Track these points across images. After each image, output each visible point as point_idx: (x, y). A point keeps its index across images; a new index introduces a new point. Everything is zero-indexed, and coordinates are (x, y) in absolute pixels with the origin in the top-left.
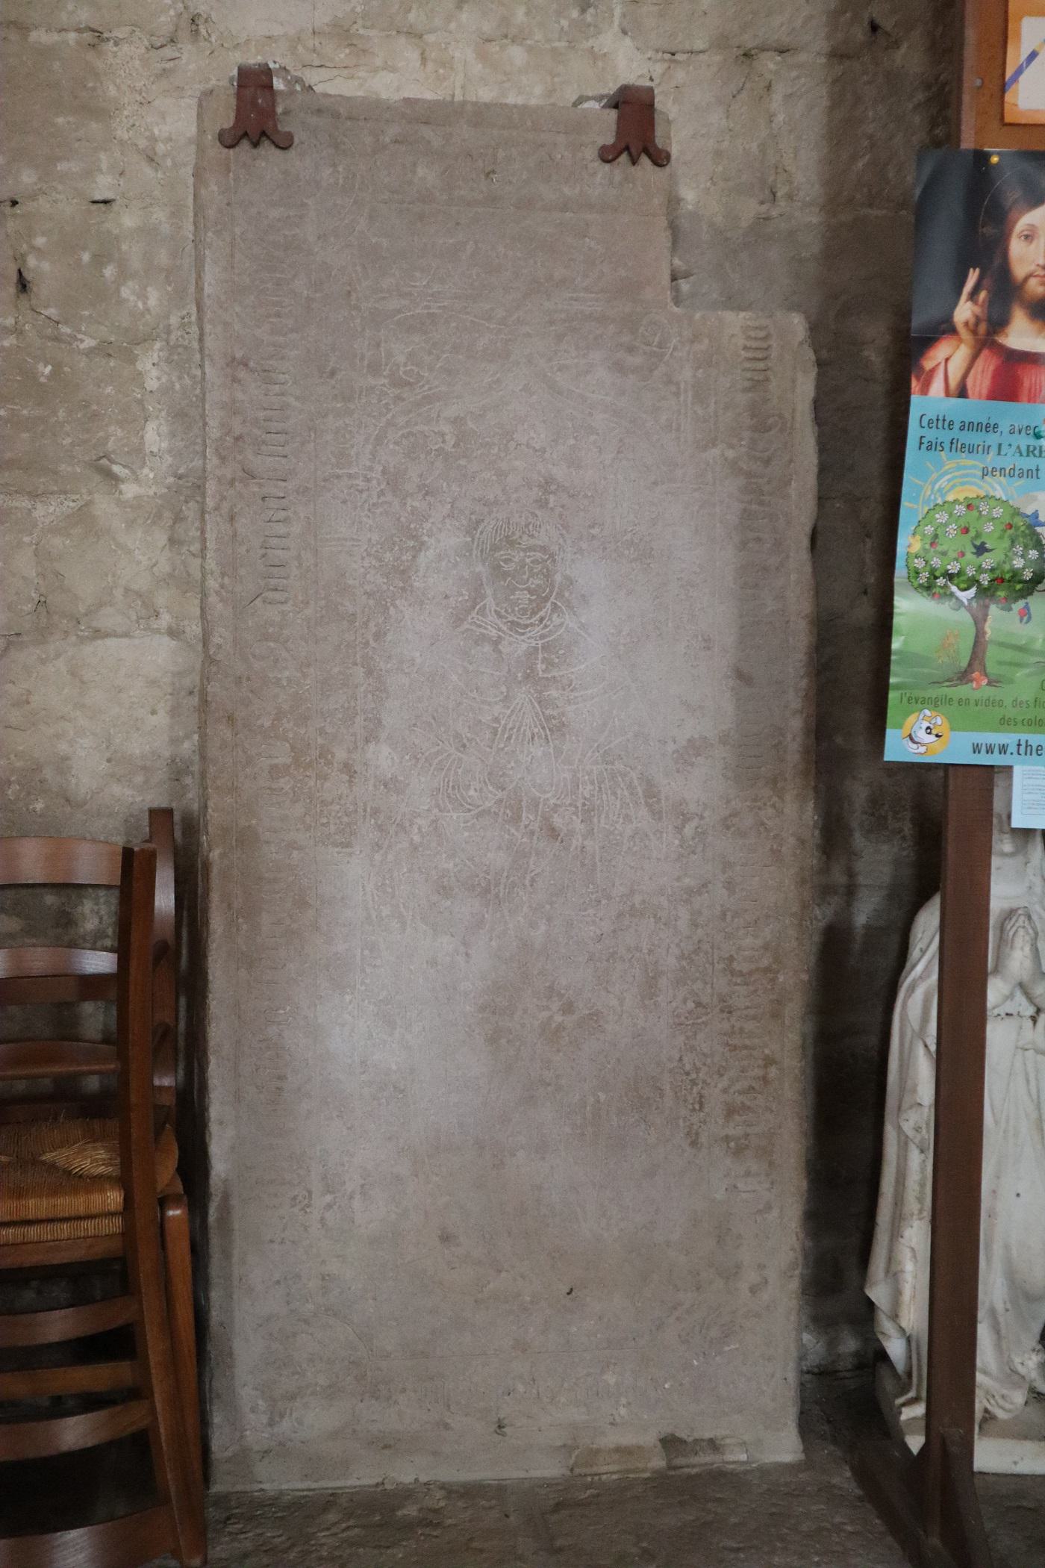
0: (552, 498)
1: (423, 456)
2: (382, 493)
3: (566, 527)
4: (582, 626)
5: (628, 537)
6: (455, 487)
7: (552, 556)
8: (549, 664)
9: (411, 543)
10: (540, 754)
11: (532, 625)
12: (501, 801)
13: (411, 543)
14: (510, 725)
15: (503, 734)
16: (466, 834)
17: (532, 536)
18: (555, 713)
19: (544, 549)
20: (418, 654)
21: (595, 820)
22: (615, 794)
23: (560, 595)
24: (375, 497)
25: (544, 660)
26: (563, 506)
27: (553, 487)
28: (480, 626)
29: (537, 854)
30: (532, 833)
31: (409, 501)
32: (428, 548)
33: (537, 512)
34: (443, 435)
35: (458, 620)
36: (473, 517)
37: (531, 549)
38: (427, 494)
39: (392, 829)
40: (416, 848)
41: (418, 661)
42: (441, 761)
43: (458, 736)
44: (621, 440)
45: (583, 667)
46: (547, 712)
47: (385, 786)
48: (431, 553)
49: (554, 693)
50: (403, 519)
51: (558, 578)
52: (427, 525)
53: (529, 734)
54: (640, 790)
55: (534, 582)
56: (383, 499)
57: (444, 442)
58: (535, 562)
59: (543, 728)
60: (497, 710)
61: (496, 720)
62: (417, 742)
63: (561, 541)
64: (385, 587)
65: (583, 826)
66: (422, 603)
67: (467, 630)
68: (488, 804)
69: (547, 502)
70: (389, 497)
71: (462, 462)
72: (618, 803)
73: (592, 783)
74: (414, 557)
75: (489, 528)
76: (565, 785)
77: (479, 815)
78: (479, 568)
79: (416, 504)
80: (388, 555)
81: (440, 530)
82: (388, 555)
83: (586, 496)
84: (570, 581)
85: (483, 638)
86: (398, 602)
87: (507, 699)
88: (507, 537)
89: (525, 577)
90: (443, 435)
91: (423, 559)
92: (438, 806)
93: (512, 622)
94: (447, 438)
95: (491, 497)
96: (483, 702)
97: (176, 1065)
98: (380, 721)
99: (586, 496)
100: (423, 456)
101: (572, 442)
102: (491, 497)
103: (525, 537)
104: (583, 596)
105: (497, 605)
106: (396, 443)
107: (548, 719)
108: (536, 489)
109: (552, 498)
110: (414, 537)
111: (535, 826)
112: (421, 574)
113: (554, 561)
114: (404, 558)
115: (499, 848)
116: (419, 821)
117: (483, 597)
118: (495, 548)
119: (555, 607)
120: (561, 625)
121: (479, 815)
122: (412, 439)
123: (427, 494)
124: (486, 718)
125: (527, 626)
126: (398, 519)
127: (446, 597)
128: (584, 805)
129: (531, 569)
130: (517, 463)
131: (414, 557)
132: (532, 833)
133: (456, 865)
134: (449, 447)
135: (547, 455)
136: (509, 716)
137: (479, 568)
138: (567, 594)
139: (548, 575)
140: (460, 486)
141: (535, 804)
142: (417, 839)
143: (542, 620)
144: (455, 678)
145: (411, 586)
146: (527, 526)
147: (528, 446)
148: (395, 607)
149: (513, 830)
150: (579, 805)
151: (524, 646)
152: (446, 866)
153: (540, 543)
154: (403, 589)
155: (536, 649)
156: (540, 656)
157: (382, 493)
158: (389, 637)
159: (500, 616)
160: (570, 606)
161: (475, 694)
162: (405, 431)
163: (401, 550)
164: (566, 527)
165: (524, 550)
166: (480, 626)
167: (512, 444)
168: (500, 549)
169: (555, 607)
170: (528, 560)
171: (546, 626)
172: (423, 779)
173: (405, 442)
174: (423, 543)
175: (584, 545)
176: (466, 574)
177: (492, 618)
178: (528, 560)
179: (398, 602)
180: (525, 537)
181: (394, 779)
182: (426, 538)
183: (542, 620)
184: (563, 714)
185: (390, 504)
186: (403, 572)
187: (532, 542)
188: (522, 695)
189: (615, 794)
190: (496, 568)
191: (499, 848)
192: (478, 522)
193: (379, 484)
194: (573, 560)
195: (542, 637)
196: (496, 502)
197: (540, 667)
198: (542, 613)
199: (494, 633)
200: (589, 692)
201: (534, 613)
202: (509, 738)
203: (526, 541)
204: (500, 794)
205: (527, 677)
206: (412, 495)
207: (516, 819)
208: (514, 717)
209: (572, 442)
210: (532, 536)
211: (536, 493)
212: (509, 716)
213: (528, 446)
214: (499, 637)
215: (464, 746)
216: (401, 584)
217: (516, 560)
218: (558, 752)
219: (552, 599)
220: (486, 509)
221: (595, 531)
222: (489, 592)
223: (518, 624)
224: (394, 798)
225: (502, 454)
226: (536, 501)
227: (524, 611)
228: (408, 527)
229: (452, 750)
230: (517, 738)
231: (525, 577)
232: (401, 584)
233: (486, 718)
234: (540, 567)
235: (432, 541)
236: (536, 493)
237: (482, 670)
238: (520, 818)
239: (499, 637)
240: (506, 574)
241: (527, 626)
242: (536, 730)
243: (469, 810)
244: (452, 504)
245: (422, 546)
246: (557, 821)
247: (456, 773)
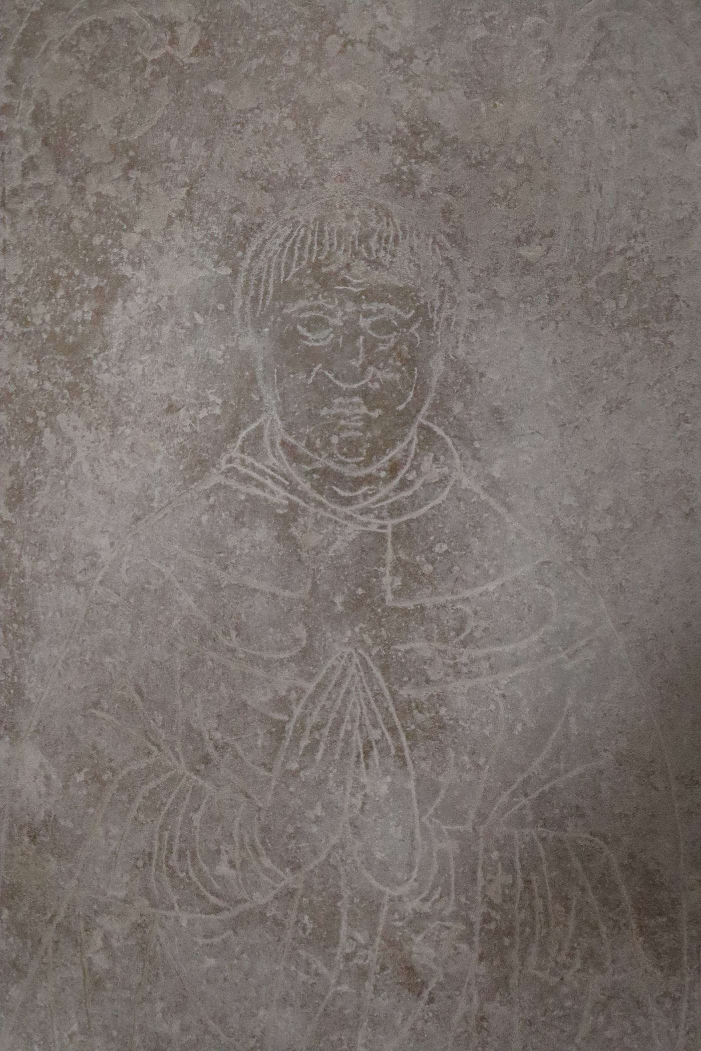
0: (426, 173)
1: (125, 78)
2: (30, 166)
3: (458, 239)
4: (493, 486)
5: (615, 266)
6: (196, 149)
7: (421, 311)
8: (411, 575)
9: (94, 282)
10: (384, 789)
11: (370, 479)
12: (291, 893)
13: (94, 282)
14: (310, 722)
15: (296, 740)
16: (211, 962)
17: (376, 264)
18: (422, 694)
19: (403, 296)
20: (104, 541)
21: (514, 957)
22: (565, 899)
23: (440, 408)
24: (17, 174)
25: (399, 566)
26: (452, 190)
27: (430, 145)
28: (247, 479)
29: (374, 1023)
30: (363, 974)
31: (92, 181)
32: (129, 295)
33: (394, 207)
34: (172, 25)
35: (200, 465)
36: (238, 218)
37: (370, 294)
38: (130, 166)
39: (49, 935)
40: (98, 984)
41: (106, 556)
42: (152, 792)
43: (192, 735)
44: (601, 25)
45: (491, 587)
46: (405, 692)
47: (33, 838)
48: (137, 304)
49: (422, 647)
50: (76, 225)
51: (438, 366)
52: (132, 238)
53: (357, 740)
54: (625, 894)
55: (381, 376)
56: (33, 179)
57: (174, 41)
58: (382, 326)
59: (393, 730)
60: (284, 680)
61: (282, 704)
62: (102, 743)
63: (446, 274)
64: (34, 384)
65: (482, 969)
66: (115, 424)
67: (218, 487)
68: (259, 899)
69: (414, 179)
70: (47, 175)
71: (216, 88)
72: (572, 923)
73: (509, 868)
74: (99, 313)
75: (274, 245)
76: (443, 870)
77: (239, 923)
78: (249, 341)
79: (108, 189)
80: (41, 308)
81: (160, 250)
82: (41, 308)
83: (510, 165)
84: (464, 375)
85: (256, 508)
86: (61, 418)
87: (307, 656)
88: (317, 266)
89: (356, 363)
90: (172, 25)
91: (121, 318)
92: (147, 893)
93: (326, 473)
94: (183, 31)
95: (282, 171)
96: (252, 660)
97: (428, 519)
98: (20, 691)
99: (510, 165)
100: (125, 78)
101: (479, 32)
102: (282, 171)
103: (359, 267)
104: (496, 411)
105: (289, 429)
106: (65, 49)
107: (406, 708)
108: (386, 150)
109: (426, 173)
110: (102, 268)
111: (372, 958)
112: (114, 351)
113: (428, 325)
114: (77, 315)
115: (285, 1001)
116: (103, 920)
117: (256, 410)
118: (286, 292)
119: (428, 438)
120: (443, 481)
121: (239, 923)
122: (102, 38)
123: (130, 166)
124: (260, 698)
125: (358, 482)
126: (67, 226)
127: (172, 409)
128: (487, 919)
129: (371, 345)
130: (346, 87)
131: (99, 313)
132: (363, 974)
133: (185, 1030)
134: (184, 56)
135: (418, 66)
136: (313, 698)
137: (249, 341)
138: (457, 407)
139: (411, 361)
140: (209, 145)
141: (370, 907)
142: (101, 962)
143: (393, 469)
144: (187, 600)
145: (92, 381)
146: (364, 238)
147: (372, 45)
148: (56, 429)
149: (318, 964)
150: (476, 917)
151: (352, 530)
152: (164, 1028)
153: (395, 281)
154: (74, 390)
155: (380, 538)
156: (390, 556)
157: (30, 166)
158: (42, 498)
159: (294, 456)
160: (463, 437)
161: (233, 641)
162: (87, 20)
163: (68, 296)
164: (458, 239)
165: (357, 299)
166: (247, 479)
167: (333, 44)
168: (299, 294)
169: (428, 438)
170: (364, 323)
171: (404, 484)
172: (115, 831)
173: (85, 45)
174: (121, 280)
175: (504, 287)
176: (217, 354)
177: (276, 460)
178: (364, 323)
179: (61, 418)
180: (359, 267)
181: (50, 822)
182: (127, 270)
183: (393, 469)
184: (442, 699)
185: (49, 189)
186: (74, 349)
187: (378, 277)
188: (342, 647)
189: (565, 899)
190: (287, 340)
191: (285, 1001)
192: (248, 232)
193: (25, 145)
194: (474, 325)
195: (396, 509)
196: (292, 182)
197: (389, 582)
198: (395, 453)
199: (280, 496)
200: (508, 648)
201: (376, 452)
202: (312, 748)
203: (360, 276)
204: (288, 879)
205: (356, 604)
206: (99, 167)
207: (324, 937)
208: (323, 700)
209: (479, 32)
210: (376, 264)
211: (388, 158)
212: (313, 698)
213: (372, 45)
214: (292, 506)
215: (206, 760)
216: (69, 378)
217: (337, 321)
218: (428, 789)
219: (420, 419)
220: (269, 199)
221: (531, 252)
222: (270, 397)
223: (339, 478)
224: (53, 865)
225: (310, 67)
226: (387, 179)
227: (351, 447)
228: (88, 246)
229: (182, 768)
230: (329, 751)
231: (356, 363)
232: (69, 378)
233: (260, 698)
234: (393, 338)
235: (142, 276)
236: (388, 158)
237: (252, 582)
238: (332, 940)
239: (292, 506)
240: (311, 356)
241: (358, 482)
242: (375, 735)
243: (217, 910)
244: (191, 186)
245: (114, 288)
246: (421, 951)
247: (188, 821)
